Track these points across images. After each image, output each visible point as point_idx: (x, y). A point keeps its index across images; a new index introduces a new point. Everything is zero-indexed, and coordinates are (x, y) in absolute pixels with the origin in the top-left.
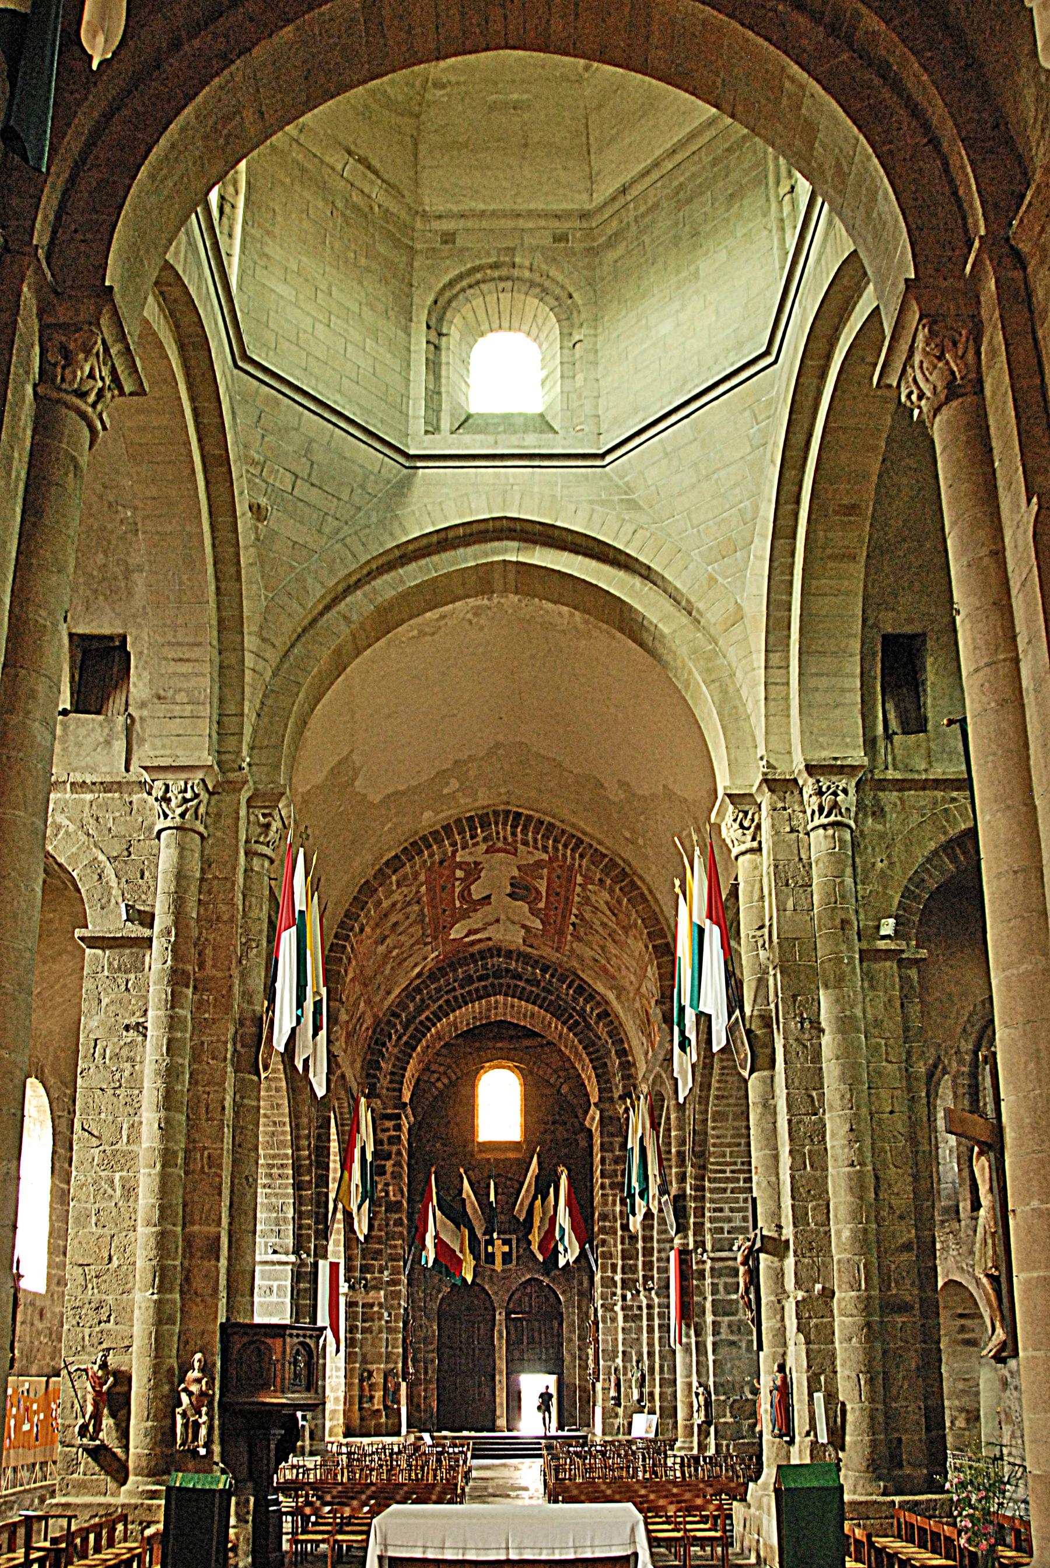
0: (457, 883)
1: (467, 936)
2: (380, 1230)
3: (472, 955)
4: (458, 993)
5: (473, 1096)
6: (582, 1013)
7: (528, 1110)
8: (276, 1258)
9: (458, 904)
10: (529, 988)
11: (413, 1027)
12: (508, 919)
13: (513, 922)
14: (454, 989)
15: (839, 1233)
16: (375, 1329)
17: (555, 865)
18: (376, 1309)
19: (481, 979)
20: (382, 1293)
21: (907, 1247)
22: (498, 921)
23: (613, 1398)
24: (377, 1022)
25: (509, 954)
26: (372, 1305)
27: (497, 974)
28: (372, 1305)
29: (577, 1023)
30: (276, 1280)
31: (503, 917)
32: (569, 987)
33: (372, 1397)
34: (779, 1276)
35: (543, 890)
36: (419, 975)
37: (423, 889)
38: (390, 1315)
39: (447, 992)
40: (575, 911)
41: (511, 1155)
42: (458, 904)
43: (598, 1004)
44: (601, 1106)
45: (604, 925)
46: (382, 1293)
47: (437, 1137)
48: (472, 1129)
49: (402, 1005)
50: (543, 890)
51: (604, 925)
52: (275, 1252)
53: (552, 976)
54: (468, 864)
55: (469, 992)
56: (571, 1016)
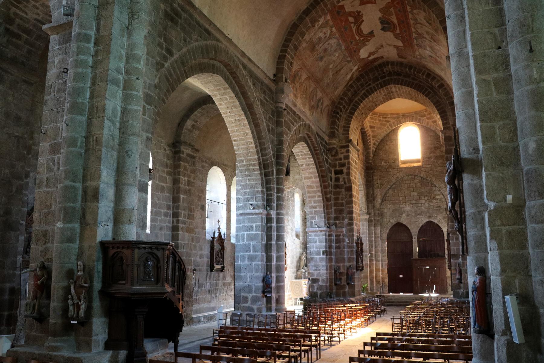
0: (352, 25)
1: (369, 56)
2: (342, 200)
3: (376, 67)
4: (371, 86)
5: (396, 140)
6: (432, 88)
7: (424, 143)
8: (253, 211)
9: (357, 38)
10: (405, 79)
11: (352, 104)
12: (388, 44)
13: (390, 45)
14: (370, 84)
15: (526, 146)
16: (342, 247)
17: (395, 3)
18: (341, 237)
19: (382, 78)
20: (344, 230)
21: (436, 199)
22: (382, 46)
23: (458, 279)
24: (333, 103)
25: (393, 63)
26: (340, 235)
27: (390, 74)
28: (340, 235)
29: (429, 93)
30: (255, 222)
31: (384, 44)
32: (423, 74)
33: (341, 279)
34: (478, 192)
35: (395, 21)
36: (351, 78)
37: (334, 29)
38: (349, 240)
39: (367, 87)
40: (414, 30)
41: (416, 164)
42: (357, 38)
43: (438, 81)
44: (445, 131)
45: (427, 33)
46: (344, 230)
47: (382, 160)
48: (394, 151)
49: (345, 94)
50: (395, 21)
51: (427, 33)
52: (254, 208)
53: (414, 71)
54: (353, 12)
55: (377, 85)
56: (426, 90)
